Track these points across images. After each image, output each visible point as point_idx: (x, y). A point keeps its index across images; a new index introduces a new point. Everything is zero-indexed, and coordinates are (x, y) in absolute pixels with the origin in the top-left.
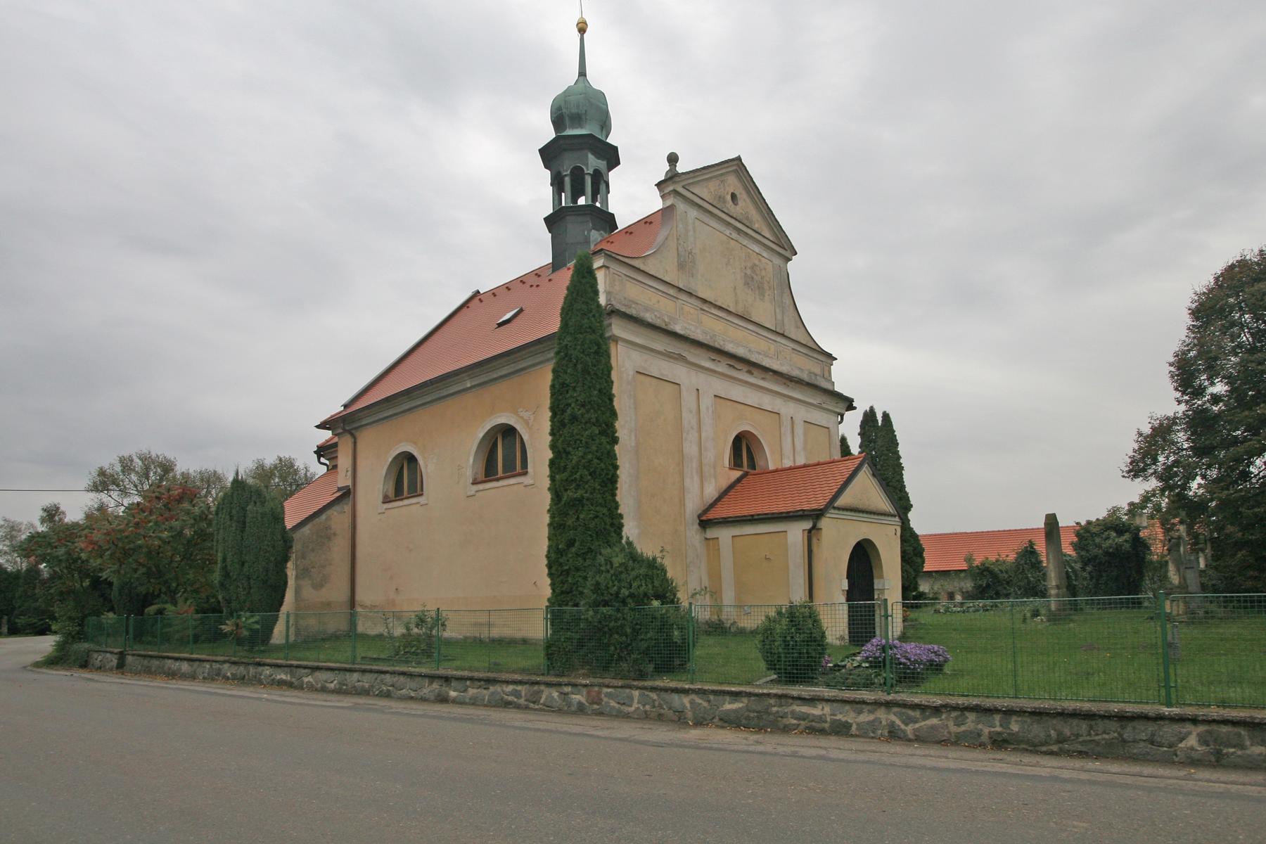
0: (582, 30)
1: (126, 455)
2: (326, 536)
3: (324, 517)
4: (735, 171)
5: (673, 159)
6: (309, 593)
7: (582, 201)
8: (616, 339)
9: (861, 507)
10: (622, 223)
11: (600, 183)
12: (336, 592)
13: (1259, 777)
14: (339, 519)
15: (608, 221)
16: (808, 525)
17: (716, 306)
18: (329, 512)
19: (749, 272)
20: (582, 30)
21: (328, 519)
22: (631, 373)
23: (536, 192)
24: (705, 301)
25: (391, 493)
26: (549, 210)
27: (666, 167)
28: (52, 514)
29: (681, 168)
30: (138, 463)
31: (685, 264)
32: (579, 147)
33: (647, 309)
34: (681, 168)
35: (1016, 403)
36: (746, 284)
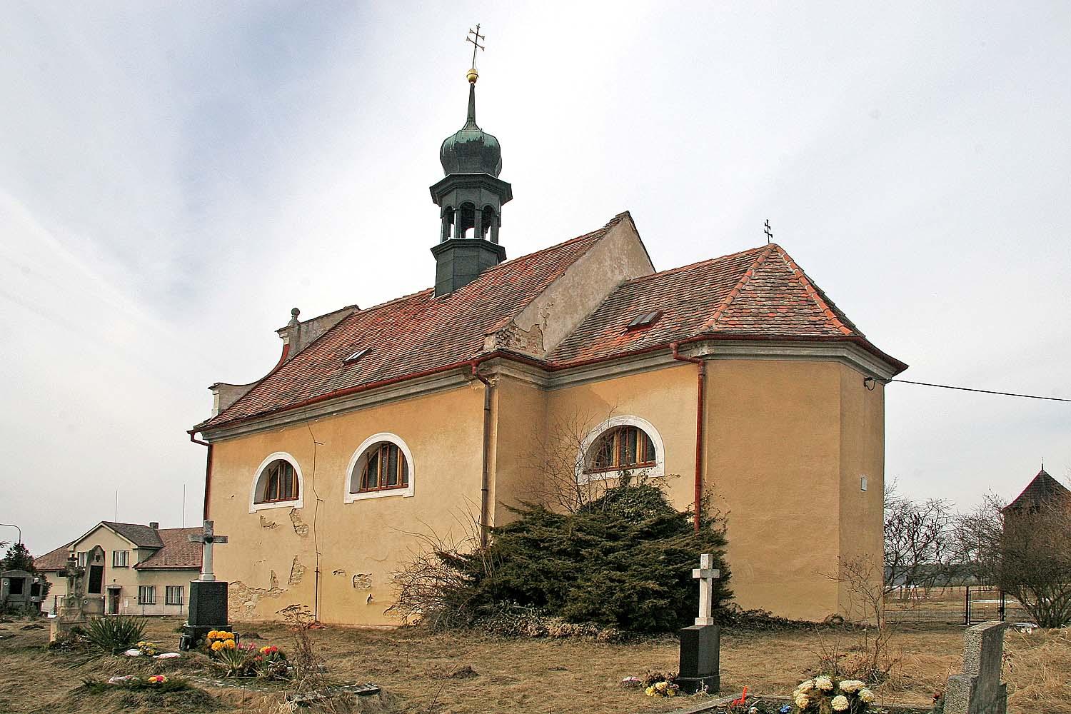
0: (473, 81)
1: (25, 546)
5: (296, 312)
7: (470, 234)
10: (511, 255)
11: (491, 219)
15: (500, 253)
20: (473, 81)
23: (428, 225)
26: (437, 241)
27: (290, 317)
29: (301, 319)
32: (471, 181)
34: (301, 319)
35: (949, 460)
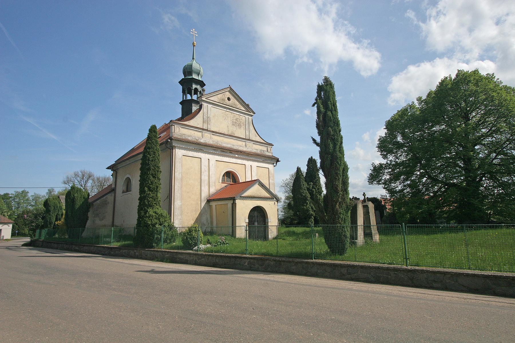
2: (105, 203)
3: (105, 197)
4: (229, 91)
6: (98, 222)
8: (175, 147)
9: (256, 196)
12: (108, 221)
13: (512, 300)
14: (110, 198)
16: (232, 202)
17: (218, 133)
18: (107, 196)
19: (234, 121)
21: (106, 198)
22: (181, 156)
24: (213, 132)
25: (125, 190)
28: (50, 191)
30: (80, 173)
31: (207, 120)
33: (189, 136)
36: (233, 125)
